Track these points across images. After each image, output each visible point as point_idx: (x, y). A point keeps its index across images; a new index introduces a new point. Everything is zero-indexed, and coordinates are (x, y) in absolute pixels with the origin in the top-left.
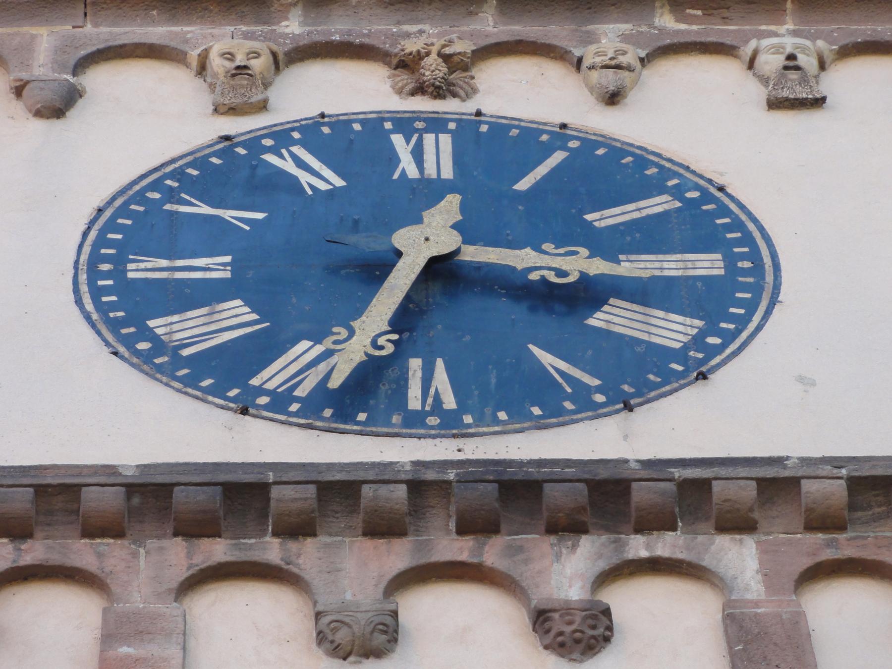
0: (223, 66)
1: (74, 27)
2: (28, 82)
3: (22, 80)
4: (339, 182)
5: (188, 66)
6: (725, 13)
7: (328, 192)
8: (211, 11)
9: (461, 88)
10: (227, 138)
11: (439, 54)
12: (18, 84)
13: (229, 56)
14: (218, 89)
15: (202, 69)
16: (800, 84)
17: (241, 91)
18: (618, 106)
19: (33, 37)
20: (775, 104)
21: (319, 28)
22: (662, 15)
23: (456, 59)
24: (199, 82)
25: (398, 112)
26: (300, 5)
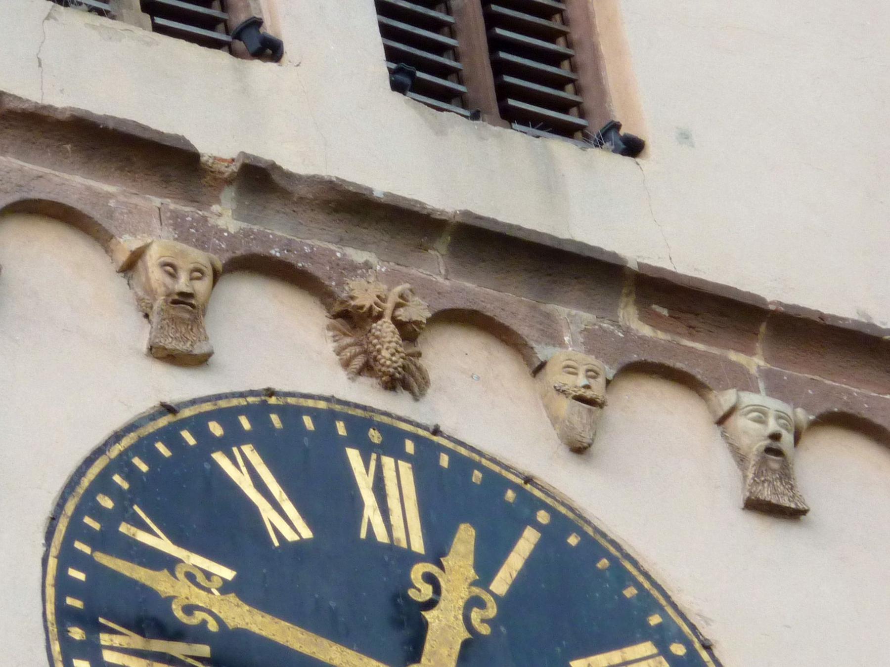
0: (165, 285)
4: (307, 533)
5: (113, 260)
6: (694, 323)
9: (416, 380)
10: (168, 409)
11: (394, 320)
13: (171, 269)
14: (155, 318)
16: (781, 479)
17: (179, 330)
18: (583, 456)
20: (756, 506)
22: (626, 306)
24: (120, 282)
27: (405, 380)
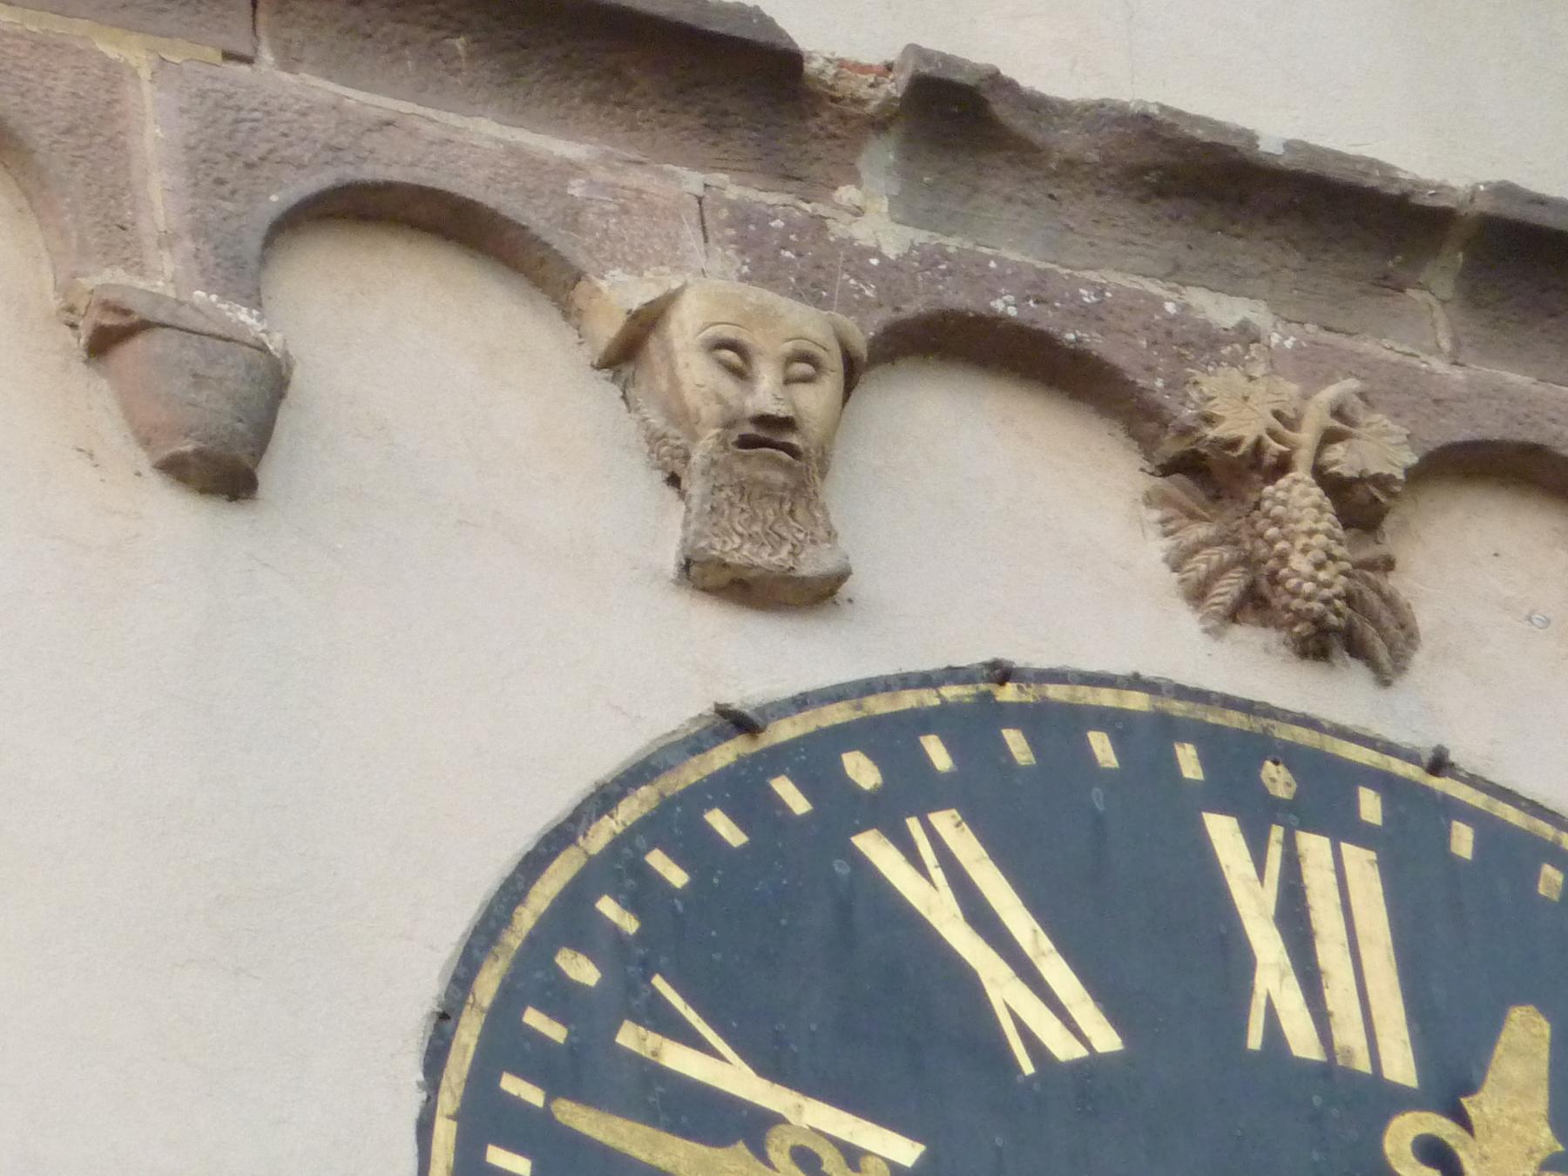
0: (720, 399)
1: (228, 56)
2: (145, 326)
3: (127, 313)
4: (1107, 1040)
7: (1077, 1065)
8: (629, 85)
10: (737, 722)
11: (1321, 475)
12: (110, 320)
13: (734, 357)
15: (629, 351)
19: (113, 73)
21: (952, 244)
23: (1360, 494)
25: (1200, 696)
26: (896, 130)
27: (1353, 632)
